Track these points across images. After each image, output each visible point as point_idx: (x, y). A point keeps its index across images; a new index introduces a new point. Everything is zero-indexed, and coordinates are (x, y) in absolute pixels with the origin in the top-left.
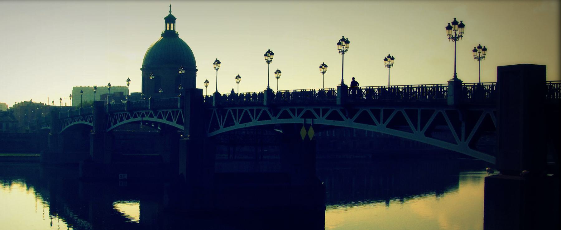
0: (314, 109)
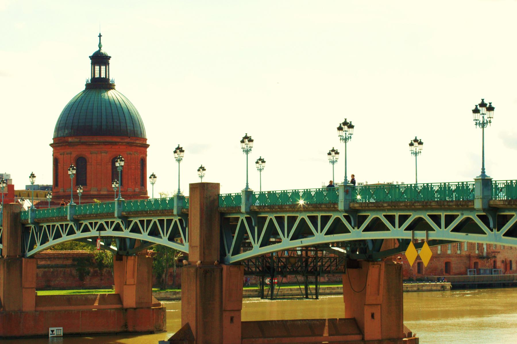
0: (385, 216)
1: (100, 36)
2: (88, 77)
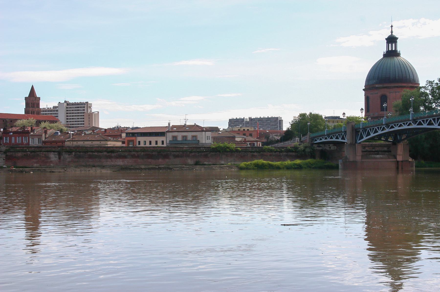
1: (392, 26)
2: (385, 50)
